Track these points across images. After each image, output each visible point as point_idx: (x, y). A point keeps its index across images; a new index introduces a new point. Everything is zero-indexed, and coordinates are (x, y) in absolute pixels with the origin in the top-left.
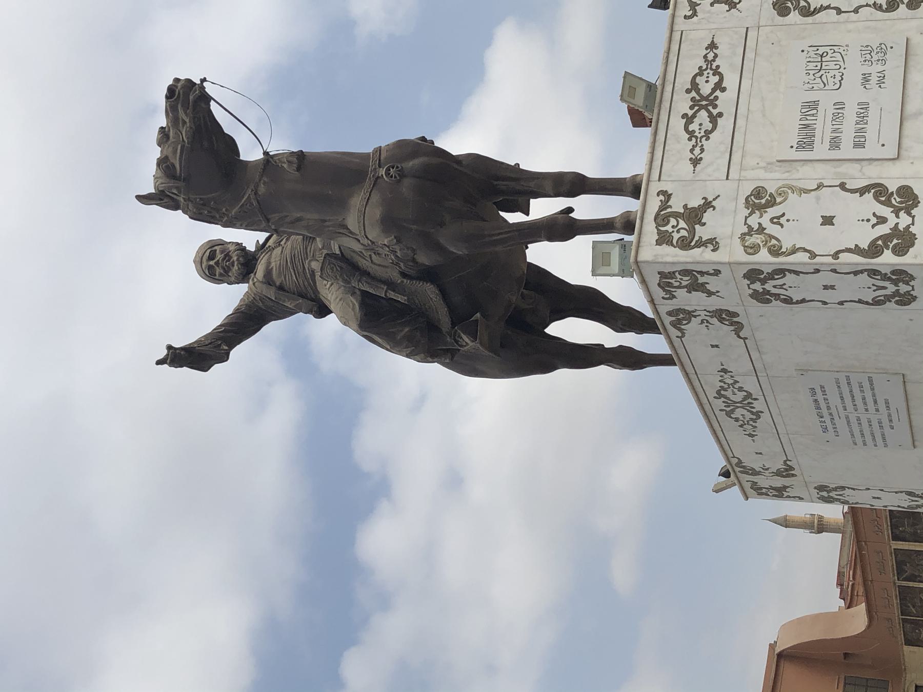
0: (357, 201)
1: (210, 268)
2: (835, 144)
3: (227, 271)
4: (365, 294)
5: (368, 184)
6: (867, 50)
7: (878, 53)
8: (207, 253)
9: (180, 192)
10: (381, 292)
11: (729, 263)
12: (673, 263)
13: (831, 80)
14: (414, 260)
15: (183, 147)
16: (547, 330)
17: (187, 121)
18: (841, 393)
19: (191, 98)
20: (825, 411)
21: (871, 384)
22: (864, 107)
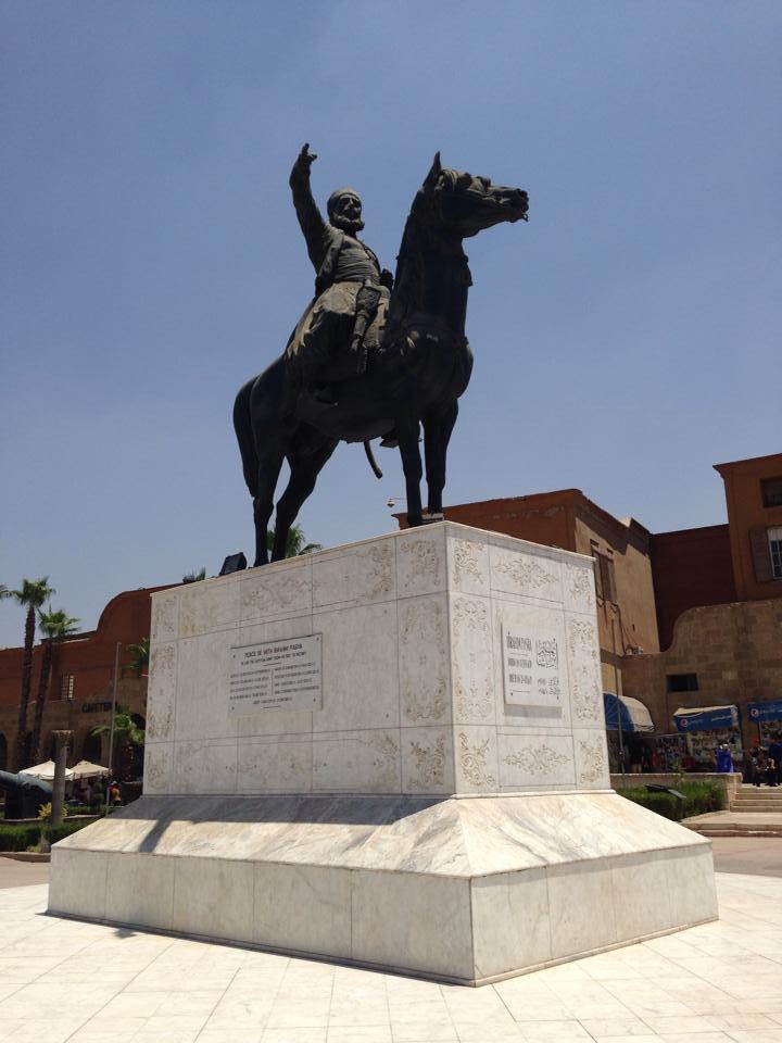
2: (512, 662)
6: (555, 681)
11: (447, 591)
16: (629, 546)
22: (528, 680)
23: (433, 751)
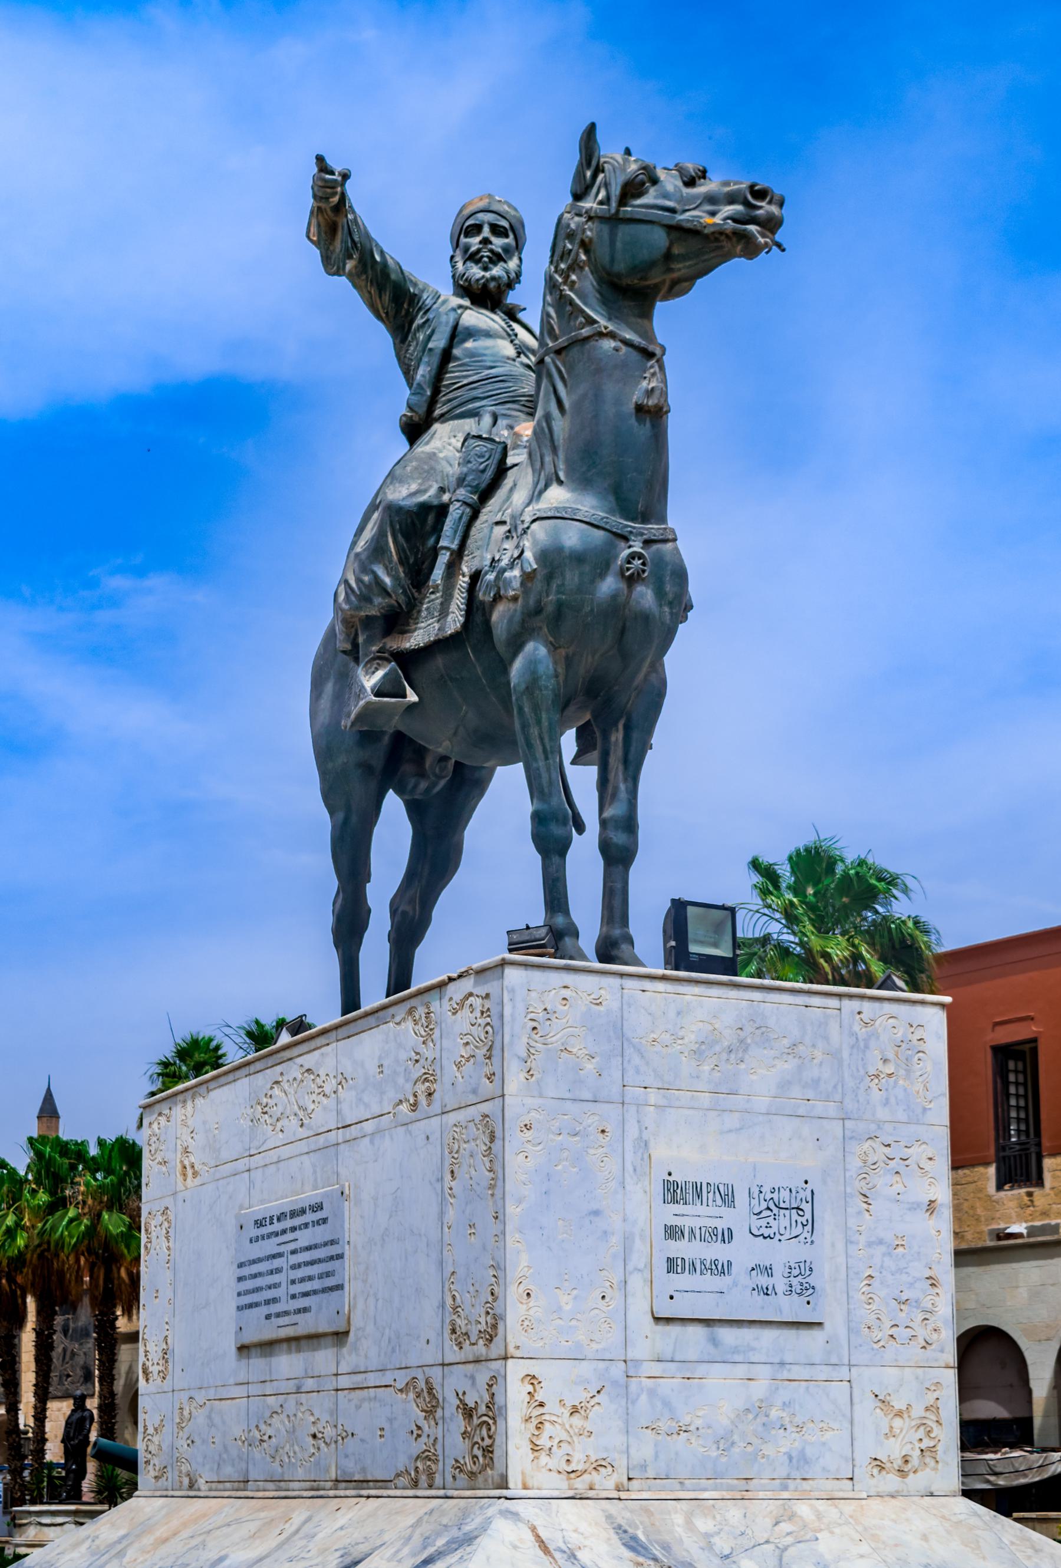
0: (588, 505)
1: (477, 228)
3: (473, 257)
4: (442, 510)
5: (619, 522)
7: (801, 1284)
8: (504, 223)
9: (601, 203)
10: (448, 540)
12: (502, 1016)
13: (763, 1223)
14: (498, 598)
15: (673, 211)
16: (391, 793)
17: (718, 220)
18: (316, 1246)
19: (753, 228)
20: (288, 1223)
21: (331, 1289)
23: (482, 1409)
